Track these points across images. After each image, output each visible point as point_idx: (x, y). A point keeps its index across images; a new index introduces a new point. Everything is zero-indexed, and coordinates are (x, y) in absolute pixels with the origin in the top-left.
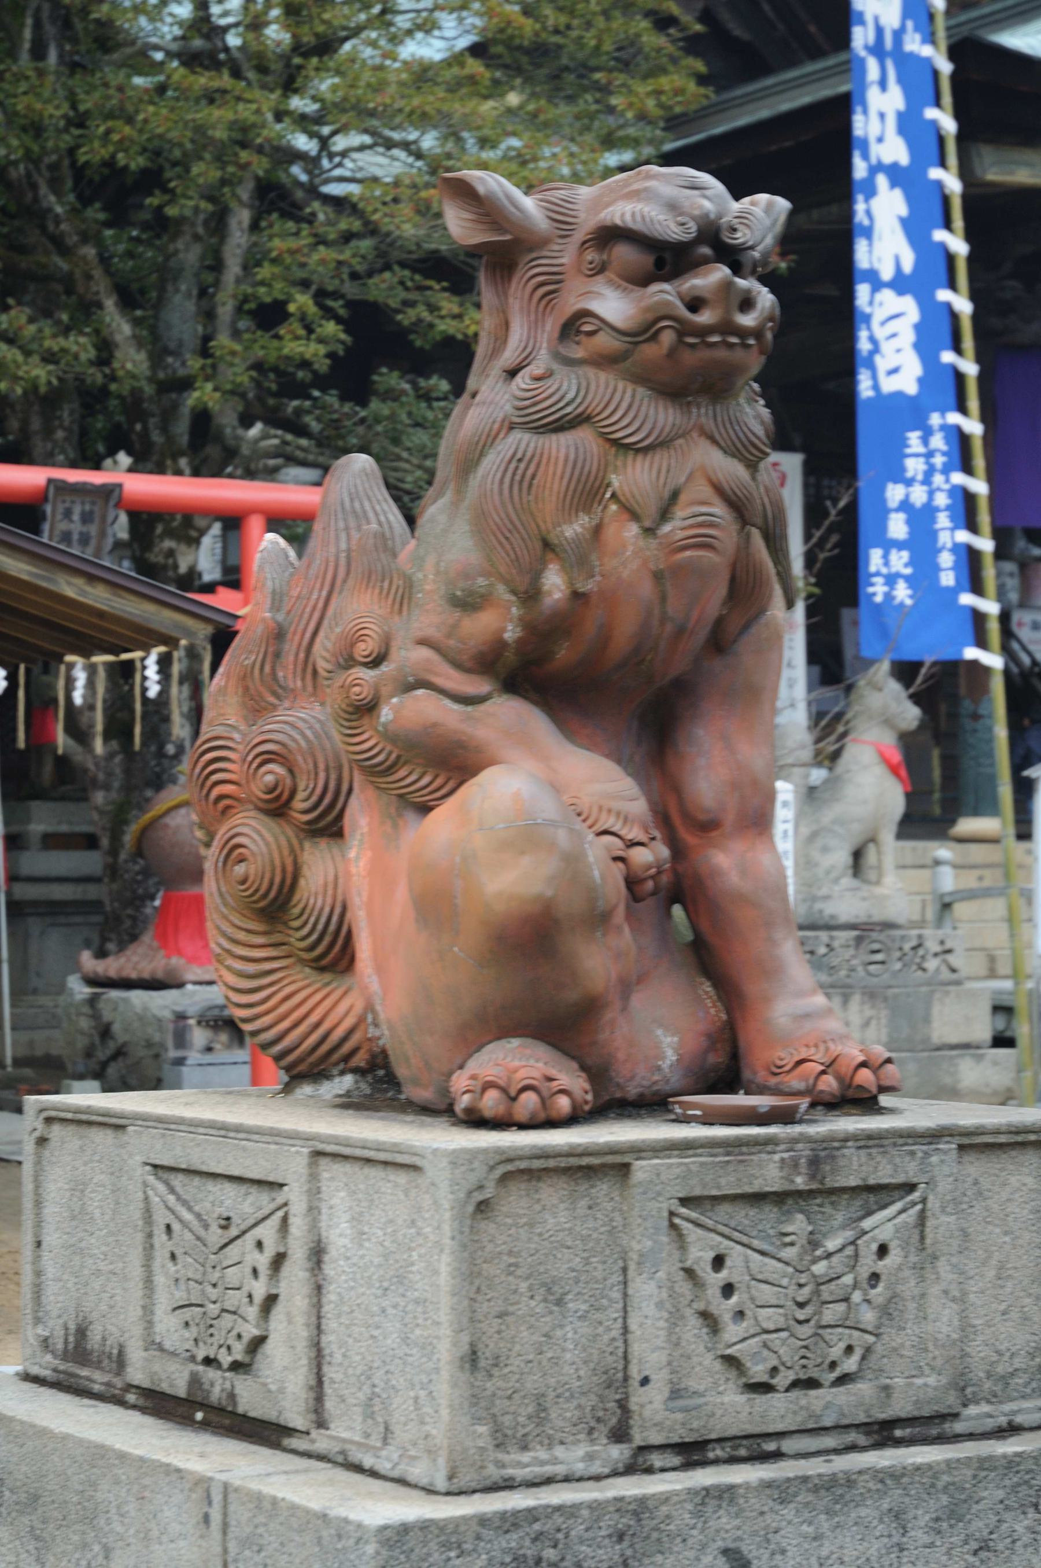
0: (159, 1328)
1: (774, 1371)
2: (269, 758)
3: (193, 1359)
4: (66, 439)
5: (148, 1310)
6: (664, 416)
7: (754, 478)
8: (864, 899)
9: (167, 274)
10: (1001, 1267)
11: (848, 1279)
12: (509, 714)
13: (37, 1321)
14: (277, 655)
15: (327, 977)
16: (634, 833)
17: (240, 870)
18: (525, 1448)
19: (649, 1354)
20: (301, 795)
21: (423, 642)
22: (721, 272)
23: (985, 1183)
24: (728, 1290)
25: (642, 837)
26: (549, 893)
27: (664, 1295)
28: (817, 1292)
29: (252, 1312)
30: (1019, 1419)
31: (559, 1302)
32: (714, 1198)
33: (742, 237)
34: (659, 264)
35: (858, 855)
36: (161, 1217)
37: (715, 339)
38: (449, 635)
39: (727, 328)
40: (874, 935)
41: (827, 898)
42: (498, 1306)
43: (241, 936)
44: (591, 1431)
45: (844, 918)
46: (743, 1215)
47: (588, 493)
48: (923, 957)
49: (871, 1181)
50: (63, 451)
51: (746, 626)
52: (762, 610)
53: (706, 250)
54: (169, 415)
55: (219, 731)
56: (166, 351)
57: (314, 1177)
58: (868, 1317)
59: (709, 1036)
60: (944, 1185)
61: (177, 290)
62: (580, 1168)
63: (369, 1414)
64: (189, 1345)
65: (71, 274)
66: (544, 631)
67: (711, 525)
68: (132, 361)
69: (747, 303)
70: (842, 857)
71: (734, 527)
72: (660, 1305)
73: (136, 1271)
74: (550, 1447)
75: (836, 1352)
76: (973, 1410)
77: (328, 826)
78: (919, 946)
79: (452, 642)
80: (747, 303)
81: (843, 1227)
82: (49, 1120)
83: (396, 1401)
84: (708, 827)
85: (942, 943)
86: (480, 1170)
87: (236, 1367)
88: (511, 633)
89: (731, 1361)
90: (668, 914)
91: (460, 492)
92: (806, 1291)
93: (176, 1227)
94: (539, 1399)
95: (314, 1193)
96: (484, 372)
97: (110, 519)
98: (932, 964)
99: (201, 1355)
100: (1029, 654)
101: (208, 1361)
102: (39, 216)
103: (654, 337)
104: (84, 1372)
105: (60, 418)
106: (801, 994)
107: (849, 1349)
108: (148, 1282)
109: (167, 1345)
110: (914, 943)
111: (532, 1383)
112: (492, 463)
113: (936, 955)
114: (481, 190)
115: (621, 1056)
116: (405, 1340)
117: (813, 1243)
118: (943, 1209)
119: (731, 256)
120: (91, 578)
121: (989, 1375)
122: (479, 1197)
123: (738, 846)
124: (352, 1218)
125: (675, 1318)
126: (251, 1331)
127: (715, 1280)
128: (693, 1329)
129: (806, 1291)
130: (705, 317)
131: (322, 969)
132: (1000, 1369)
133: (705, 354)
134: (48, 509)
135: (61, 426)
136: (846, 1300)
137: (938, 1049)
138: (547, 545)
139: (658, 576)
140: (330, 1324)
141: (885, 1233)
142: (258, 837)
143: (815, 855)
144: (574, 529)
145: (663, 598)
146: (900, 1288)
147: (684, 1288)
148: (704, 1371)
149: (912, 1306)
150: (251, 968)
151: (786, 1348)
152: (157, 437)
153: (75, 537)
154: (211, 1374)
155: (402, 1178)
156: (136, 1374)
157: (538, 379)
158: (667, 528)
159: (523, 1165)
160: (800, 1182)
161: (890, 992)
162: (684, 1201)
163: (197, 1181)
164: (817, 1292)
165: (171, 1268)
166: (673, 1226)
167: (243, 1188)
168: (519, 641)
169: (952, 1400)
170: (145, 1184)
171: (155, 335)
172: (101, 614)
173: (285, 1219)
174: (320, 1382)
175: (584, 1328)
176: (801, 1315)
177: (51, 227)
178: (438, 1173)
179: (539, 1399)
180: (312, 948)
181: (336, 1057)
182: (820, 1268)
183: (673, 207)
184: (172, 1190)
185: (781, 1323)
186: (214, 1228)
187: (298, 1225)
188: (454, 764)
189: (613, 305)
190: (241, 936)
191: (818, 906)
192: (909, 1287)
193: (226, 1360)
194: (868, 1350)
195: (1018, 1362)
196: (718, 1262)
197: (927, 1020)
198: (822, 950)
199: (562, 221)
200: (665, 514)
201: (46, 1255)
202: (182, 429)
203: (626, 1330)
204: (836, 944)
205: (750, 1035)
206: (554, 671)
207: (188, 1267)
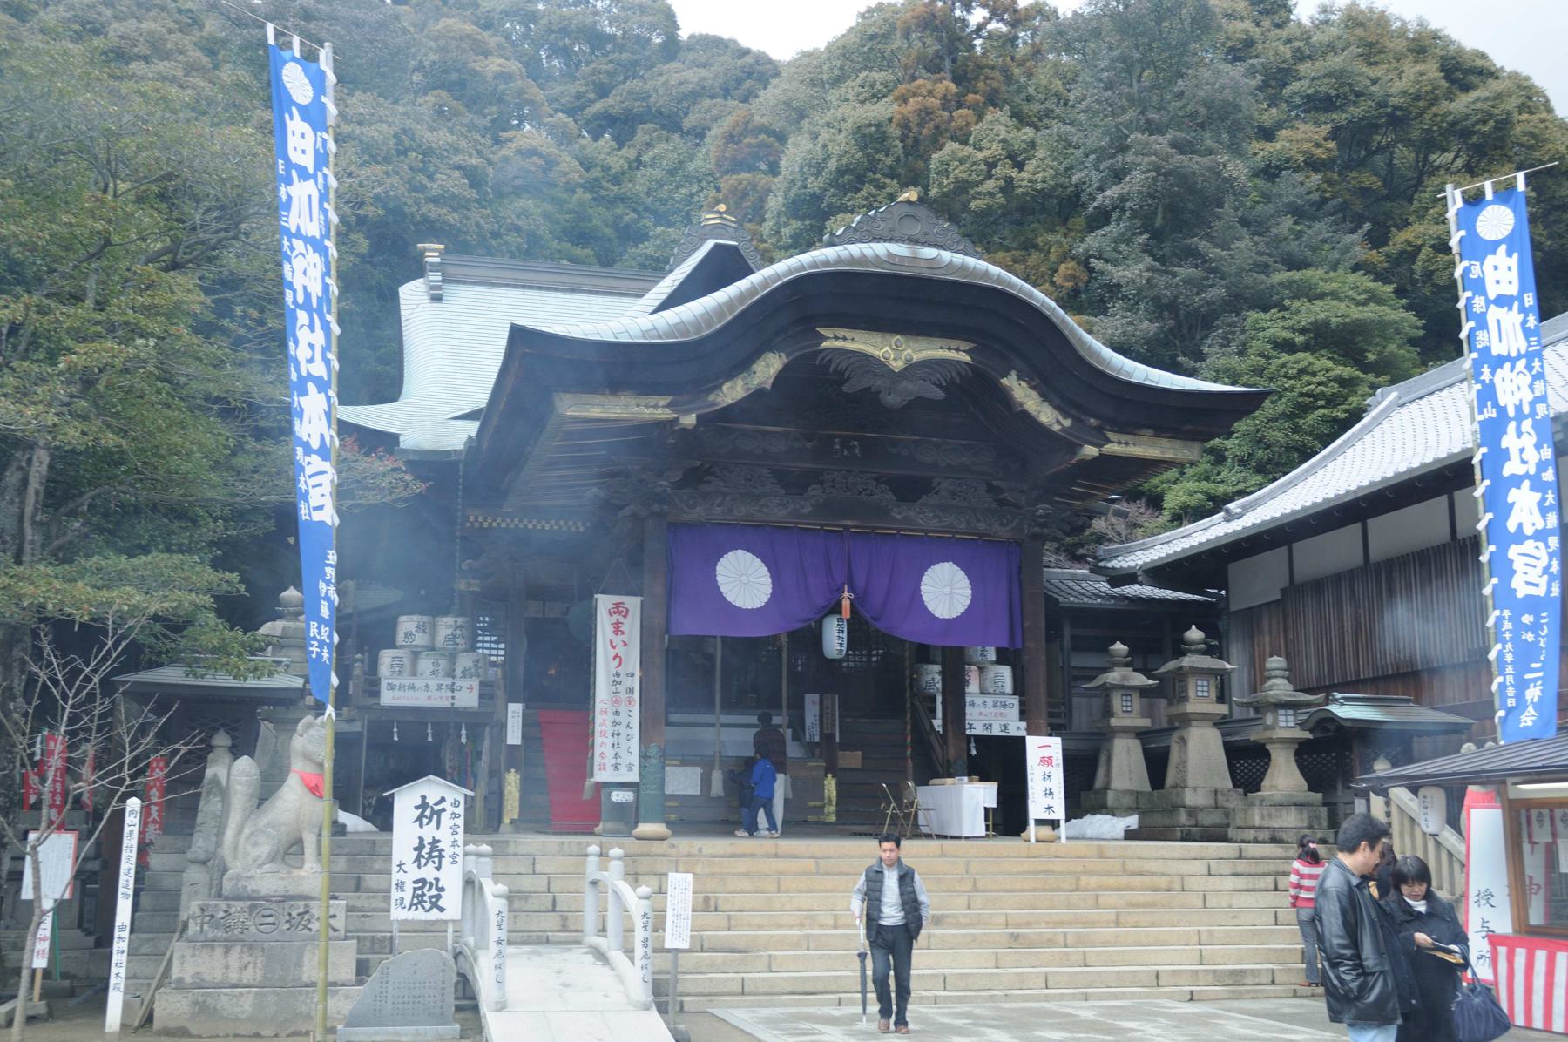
161: (266, 945)
197: (299, 965)
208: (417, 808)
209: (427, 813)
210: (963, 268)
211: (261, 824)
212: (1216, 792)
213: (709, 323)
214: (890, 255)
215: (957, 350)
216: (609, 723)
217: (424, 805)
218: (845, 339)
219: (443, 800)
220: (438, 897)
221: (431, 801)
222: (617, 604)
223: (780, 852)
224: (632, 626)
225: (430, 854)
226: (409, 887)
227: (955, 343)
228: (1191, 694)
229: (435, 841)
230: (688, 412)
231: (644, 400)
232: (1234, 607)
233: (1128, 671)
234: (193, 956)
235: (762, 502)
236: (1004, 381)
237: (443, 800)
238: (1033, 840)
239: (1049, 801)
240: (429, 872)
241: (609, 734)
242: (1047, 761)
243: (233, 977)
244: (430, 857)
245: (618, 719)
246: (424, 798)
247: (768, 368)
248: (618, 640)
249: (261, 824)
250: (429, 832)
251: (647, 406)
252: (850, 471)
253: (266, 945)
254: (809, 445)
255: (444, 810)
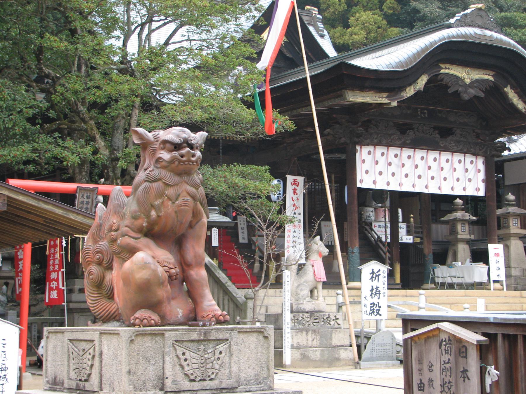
0: (71, 375)
1: (196, 377)
2: (98, 252)
3: (77, 380)
4: (86, 175)
5: (68, 371)
6: (177, 179)
7: (197, 191)
8: (313, 304)
9: (114, 129)
10: (248, 357)
11: (213, 359)
12: (144, 241)
13: (46, 377)
14: (100, 230)
15: (110, 300)
16: (171, 266)
17: (91, 277)
18: (141, 391)
19: (168, 373)
20: (105, 260)
21: (126, 226)
22: (188, 149)
23: (245, 340)
24: (186, 360)
25: (173, 267)
26: (149, 278)
27: (171, 360)
28: (206, 361)
29: (88, 368)
30: (251, 389)
31: (149, 361)
32: (183, 341)
33: (193, 142)
34: (175, 148)
35: (312, 291)
36: (71, 350)
37: (187, 163)
38: (132, 225)
39: (189, 161)
40: (315, 314)
41: (302, 304)
42: (135, 362)
43: (92, 292)
44: (155, 388)
45: (307, 310)
46: (189, 344)
47: (160, 194)
48: (330, 321)
49: (218, 338)
50: (85, 178)
51: (197, 223)
52: (200, 219)
53: (185, 145)
54: (114, 168)
55: (88, 246)
56: (115, 150)
57: (100, 338)
58: (217, 367)
59: (190, 310)
60: (234, 339)
61: (118, 133)
62: (153, 334)
63: (110, 387)
64: (76, 377)
65: (87, 129)
66: (152, 224)
67: (187, 201)
68: (104, 153)
69: (193, 156)
70: (306, 292)
71: (193, 202)
72: (170, 362)
73: (66, 363)
74: (146, 391)
75: (210, 374)
76: (241, 387)
77: (110, 268)
78: (329, 317)
79: (132, 226)
80: (193, 156)
81: (212, 348)
82: (49, 333)
83: (115, 383)
84: (189, 266)
85: (335, 316)
86: (131, 334)
87: (86, 380)
88: (145, 224)
89: (186, 375)
90: (183, 284)
91: (134, 196)
92: (203, 361)
93: (74, 352)
94: (144, 381)
95: (100, 341)
96: (141, 170)
97: (95, 198)
98: (332, 323)
99: (78, 379)
100: (377, 235)
101: (80, 380)
102: (78, 113)
103: (174, 163)
104: (56, 387)
105: (84, 169)
106: (209, 301)
107: (213, 373)
108: (69, 365)
109: (72, 378)
110: (327, 316)
111: (143, 378)
112: (141, 188)
113: (333, 320)
114: (139, 132)
115: (168, 313)
116: (117, 370)
117: (205, 350)
118: (234, 345)
119: (191, 147)
120: (78, 214)
121: (245, 380)
122: (131, 339)
123: (196, 269)
124: (108, 346)
125: (174, 365)
126: (88, 372)
127: (183, 358)
128: (178, 368)
129: (203, 361)
130: (184, 159)
131: (110, 299)
132: (248, 379)
133: (184, 166)
134: (77, 195)
135: (84, 171)
136: (212, 363)
137: (334, 347)
138: (152, 206)
139: (176, 212)
140: (103, 369)
141: (221, 349)
142: (94, 269)
143: (299, 291)
144: (158, 202)
145: (177, 217)
146: (224, 361)
147: (176, 359)
148: (180, 377)
149: (228, 365)
150: (94, 299)
151: (198, 373)
152: (111, 174)
153: (85, 203)
154: (81, 383)
155: (116, 336)
156: (66, 386)
157: (150, 171)
158: (177, 202)
159: (140, 333)
160: (202, 338)
161: (320, 331)
162: (176, 341)
163: (78, 342)
164: (206, 361)
165: (73, 361)
166: (174, 346)
167: (87, 342)
168: (147, 226)
169: (236, 385)
170: (68, 344)
171: (111, 146)
172: (81, 223)
173: (95, 348)
174: (101, 381)
175: (154, 367)
176: (202, 366)
177: (81, 116)
178: (122, 334)
179: (144, 381)
180: (107, 293)
181: (112, 318)
182: (206, 356)
183: (178, 136)
184: (73, 345)
185: (197, 367)
186: (81, 351)
187: (97, 349)
188: (132, 251)
189: (166, 156)
190: (92, 292)
191: (299, 306)
192: (227, 360)
193: (83, 379)
194: (217, 373)
195: (252, 378)
196: (184, 354)
197: (331, 339)
198: (301, 319)
199: (156, 138)
200: (177, 199)
201: (48, 362)
202: (119, 172)
203: (163, 368)
204: (304, 317)
205: (198, 310)
206: (155, 233)
207: (76, 360)
208: (371, 274)
209: (374, 275)
210: (501, 41)
211: (302, 282)
212: (523, 270)
213: (411, 62)
214: (475, 33)
215: (489, 75)
216: (291, 236)
217: (373, 273)
218: (449, 69)
219: (379, 270)
220: (379, 310)
221: (375, 271)
222: (295, 180)
223: (408, 295)
224: (301, 190)
225: (376, 292)
226: (369, 306)
227: (488, 72)
228: (511, 224)
229: (377, 287)
230: (394, 100)
231: (378, 95)
232: (507, 183)
233: (463, 212)
234: (296, 335)
235: (392, 137)
236: (505, 89)
237: (379, 270)
238: (492, 289)
239: (498, 272)
240: (375, 300)
241: (291, 242)
242: (497, 255)
243: (310, 344)
244: (376, 294)
245: (295, 235)
246: (373, 270)
247: (422, 82)
248: (295, 197)
249: (302, 282)
250: (375, 284)
251: (379, 98)
252: (424, 124)
253: (320, 331)
254: (409, 112)
255: (380, 275)
